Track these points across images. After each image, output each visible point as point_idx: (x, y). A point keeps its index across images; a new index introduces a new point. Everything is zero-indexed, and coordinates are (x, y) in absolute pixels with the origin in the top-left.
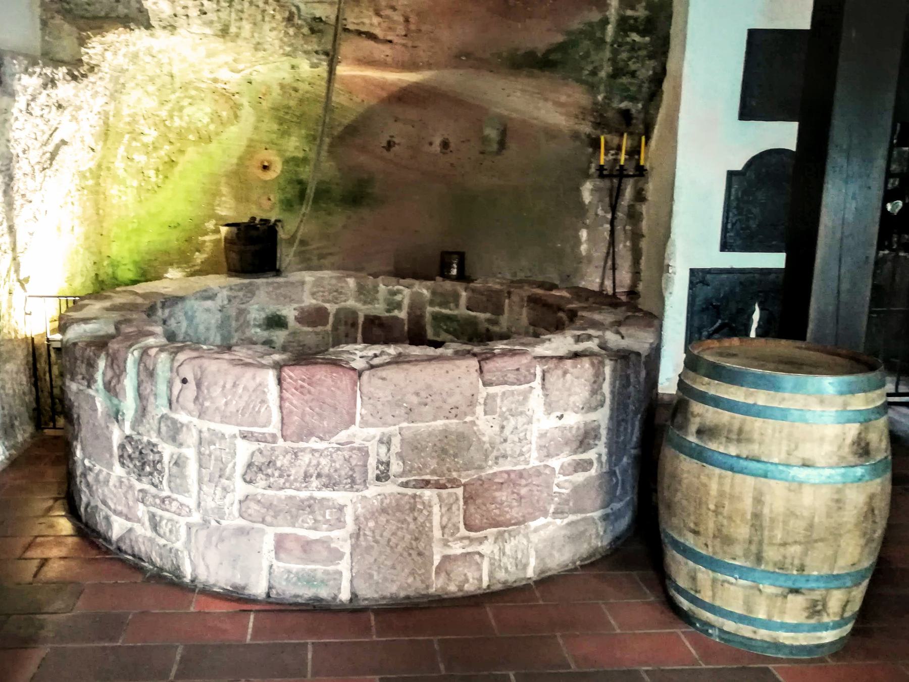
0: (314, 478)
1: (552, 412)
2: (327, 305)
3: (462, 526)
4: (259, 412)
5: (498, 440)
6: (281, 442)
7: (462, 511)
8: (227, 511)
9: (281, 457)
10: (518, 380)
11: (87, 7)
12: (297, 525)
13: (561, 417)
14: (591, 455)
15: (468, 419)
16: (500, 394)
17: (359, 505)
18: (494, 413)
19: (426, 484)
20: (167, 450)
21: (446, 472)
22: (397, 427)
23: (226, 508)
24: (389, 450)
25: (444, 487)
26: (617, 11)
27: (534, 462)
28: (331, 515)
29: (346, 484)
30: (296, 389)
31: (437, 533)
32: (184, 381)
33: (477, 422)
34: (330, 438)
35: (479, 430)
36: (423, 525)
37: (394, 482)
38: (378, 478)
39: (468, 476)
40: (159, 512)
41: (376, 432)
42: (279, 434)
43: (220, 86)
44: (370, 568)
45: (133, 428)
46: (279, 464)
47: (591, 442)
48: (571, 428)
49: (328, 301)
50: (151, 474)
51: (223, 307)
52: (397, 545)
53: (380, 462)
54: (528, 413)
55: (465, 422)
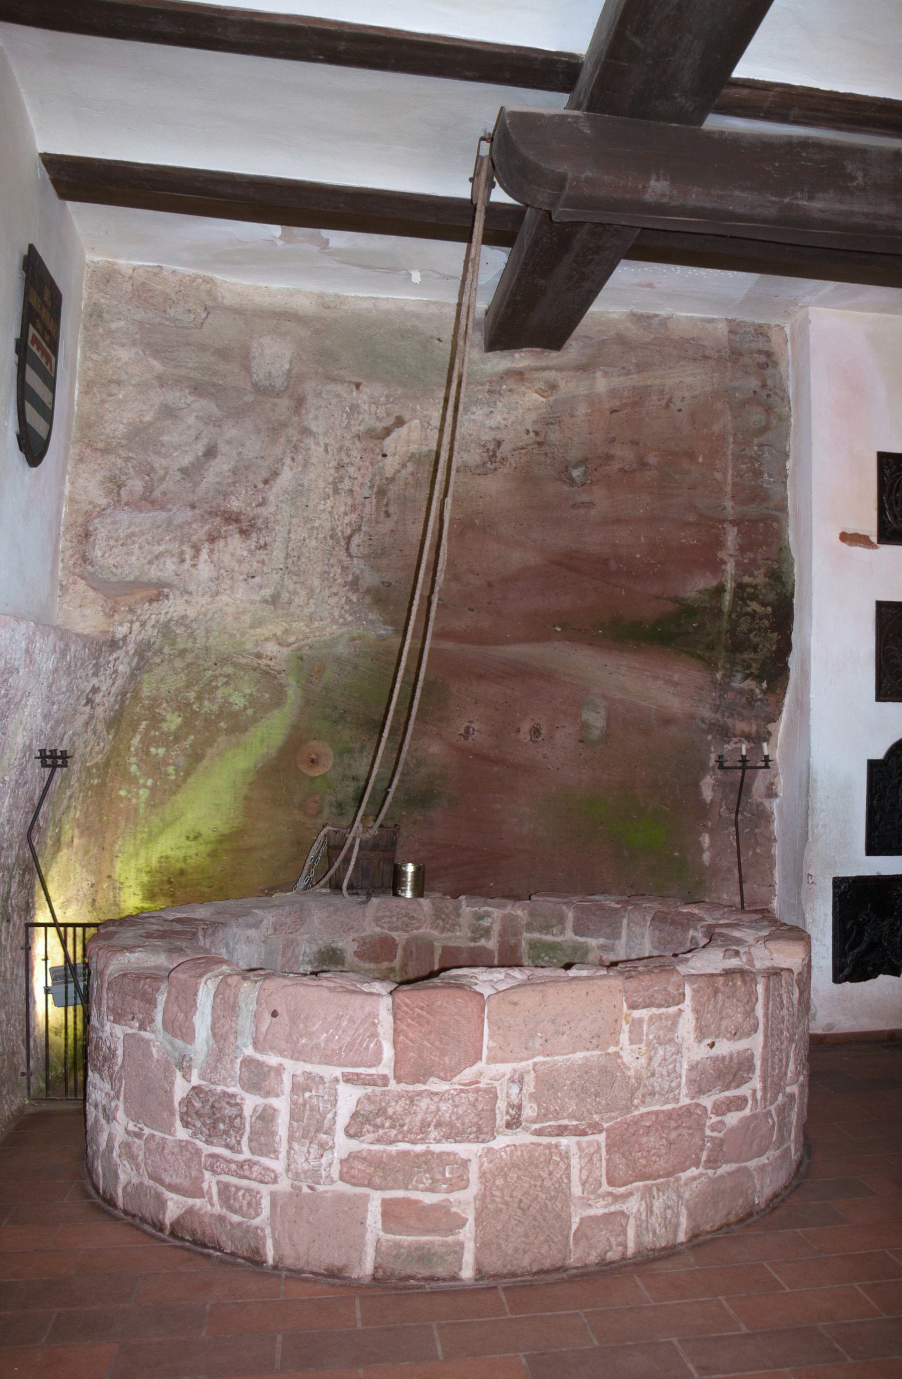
0: (432, 1128)
1: (704, 1038)
2: (394, 934)
3: (604, 1180)
4: (367, 1048)
5: (647, 1073)
6: (393, 1085)
7: (604, 1163)
8: (324, 1174)
9: (393, 1103)
10: (666, 1001)
11: (114, 569)
12: (410, 1187)
13: (712, 1045)
14: (745, 1090)
15: (612, 1049)
16: (646, 1018)
17: (485, 1159)
18: (640, 1041)
19: (561, 1131)
20: (251, 1103)
21: (585, 1114)
22: (530, 1062)
23: (322, 1169)
24: (521, 1090)
25: (584, 1133)
26: (734, 578)
27: (685, 1101)
28: (451, 1173)
29: (470, 1133)
30: (413, 1019)
31: (577, 1190)
32: (274, 1014)
33: (621, 1053)
34: (452, 1077)
35: (623, 1063)
36: (559, 1181)
37: (526, 1129)
38: (509, 1125)
39: (611, 1118)
40: (234, 1180)
41: (507, 1068)
42: (391, 1075)
43: (263, 662)
44: (498, 1237)
45: (202, 1077)
46: (390, 1111)
47: (745, 1075)
48: (724, 1058)
49: (396, 929)
50: (226, 1132)
51: (267, 938)
52: (529, 1206)
53: (510, 1105)
54: (676, 1041)
55: (609, 1054)
